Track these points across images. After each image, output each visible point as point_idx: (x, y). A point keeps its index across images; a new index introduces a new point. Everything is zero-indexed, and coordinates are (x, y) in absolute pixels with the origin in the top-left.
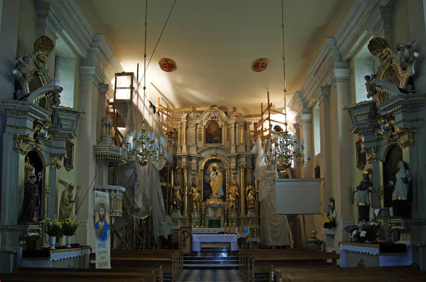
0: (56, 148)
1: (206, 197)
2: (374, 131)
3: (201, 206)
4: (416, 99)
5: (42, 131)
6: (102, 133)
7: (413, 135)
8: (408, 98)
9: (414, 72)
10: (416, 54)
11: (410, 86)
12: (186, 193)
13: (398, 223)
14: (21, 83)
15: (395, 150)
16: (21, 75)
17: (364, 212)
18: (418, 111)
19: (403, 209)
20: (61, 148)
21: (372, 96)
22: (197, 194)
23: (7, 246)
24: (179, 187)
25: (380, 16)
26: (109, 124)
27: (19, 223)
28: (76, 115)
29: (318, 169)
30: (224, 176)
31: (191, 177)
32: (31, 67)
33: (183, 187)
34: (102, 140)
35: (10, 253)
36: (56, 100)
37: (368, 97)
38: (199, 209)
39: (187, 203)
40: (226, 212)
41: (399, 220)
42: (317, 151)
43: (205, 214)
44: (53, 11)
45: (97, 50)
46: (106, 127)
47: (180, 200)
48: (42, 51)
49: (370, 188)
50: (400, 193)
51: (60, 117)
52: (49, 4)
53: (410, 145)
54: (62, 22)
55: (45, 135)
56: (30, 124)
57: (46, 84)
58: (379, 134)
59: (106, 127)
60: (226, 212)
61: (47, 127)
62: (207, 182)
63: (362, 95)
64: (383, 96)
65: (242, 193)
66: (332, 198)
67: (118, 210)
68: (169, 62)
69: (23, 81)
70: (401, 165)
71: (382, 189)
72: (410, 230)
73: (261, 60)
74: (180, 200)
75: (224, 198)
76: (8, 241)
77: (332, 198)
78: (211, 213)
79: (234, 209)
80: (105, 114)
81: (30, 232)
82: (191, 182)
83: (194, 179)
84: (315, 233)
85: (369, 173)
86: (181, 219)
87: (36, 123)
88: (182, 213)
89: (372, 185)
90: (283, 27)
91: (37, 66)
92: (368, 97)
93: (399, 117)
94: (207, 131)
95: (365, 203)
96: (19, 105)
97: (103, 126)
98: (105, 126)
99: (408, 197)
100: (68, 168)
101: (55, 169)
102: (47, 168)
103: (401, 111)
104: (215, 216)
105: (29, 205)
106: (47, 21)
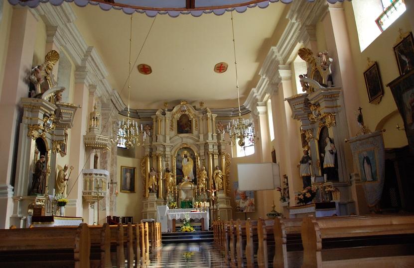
0: (57, 136)
1: (179, 181)
2: (308, 116)
3: (175, 189)
4: (333, 91)
5: (48, 122)
6: (90, 126)
7: (335, 118)
8: (328, 90)
9: (331, 72)
10: (331, 60)
11: (330, 82)
12: (161, 178)
13: (329, 185)
14: (35, 85)
15: (325, 130)
16: (36, 79)
17: (307, 180)
18: (336, 100)
19: (332, 174)
20: (61, 136)
21: (306, 90)
22: (171, 178)
23: (18, 213)
24: (154, 173)
25: (306, 32)
26: (97, 118)
27: (29, 194)
28: (74, 110)
29: (274, 153)
30: (195, 162)
31: (165, 163)
32: (42, 74)
33: (158, 172)
34: (90, 131)
35: (20, 218)
36: (59, 98)
37: (303, 91)
38: (173, 192)
39: (162, 187)
40: (196, 194)
41: (330, 183)
42: (272, 138)
43: (178, 197)
44: (60, 32)
45: (90, 58)
46: (94, 120)
47: (156, 184)
48: (51, 61)
49: (310, 161)
50: (329, 162)
51: (61, 111)
52: (57, 27)
53: (333, 125)
54: (65, 40)
55: (50, 124)
56: (41, 115)
57: (52, 86)
58: (312, 119)
59: (94, 120)
60: (196, 194)
61: (52, 119)
62: (179, 168)
63: (300, 90)
64: (313, 90)
65: (211, 178)
66: (285, 175)
67: (103, 191)
68: (146, 67)
69: (36, 84)
70: (328, 140)
71: (319, 161)
72: (338, 190)
73: (222, 64)
74: (156, 184)
75: (195, 181)
76: (19, 210)
77: (285, 175)
78: (183, 196)
79: (204, 191)
80: (93, 110)
81: (37, 201)
82: (165, 168)
83: (167, 165)
84: (274, 207)
85: (308, 150)
86: (156, 202)
87: (45, 116)
88: (158, 196)
89: (311, 160)
90: (234, 41)
91: (46, 73)
92: (304, 91)
93: (323, 104)
94: (179, 122)
95: (307, 174)
96: (33, 101)
97: (91, 119)
98: (93, 119)
99: (334, 165)
100: (62, 154)
101: (56, 153)
102: (50, 152)
103: (323, 100)
104: (187, 198)
105: (38, 180)
106: (54, 39)
